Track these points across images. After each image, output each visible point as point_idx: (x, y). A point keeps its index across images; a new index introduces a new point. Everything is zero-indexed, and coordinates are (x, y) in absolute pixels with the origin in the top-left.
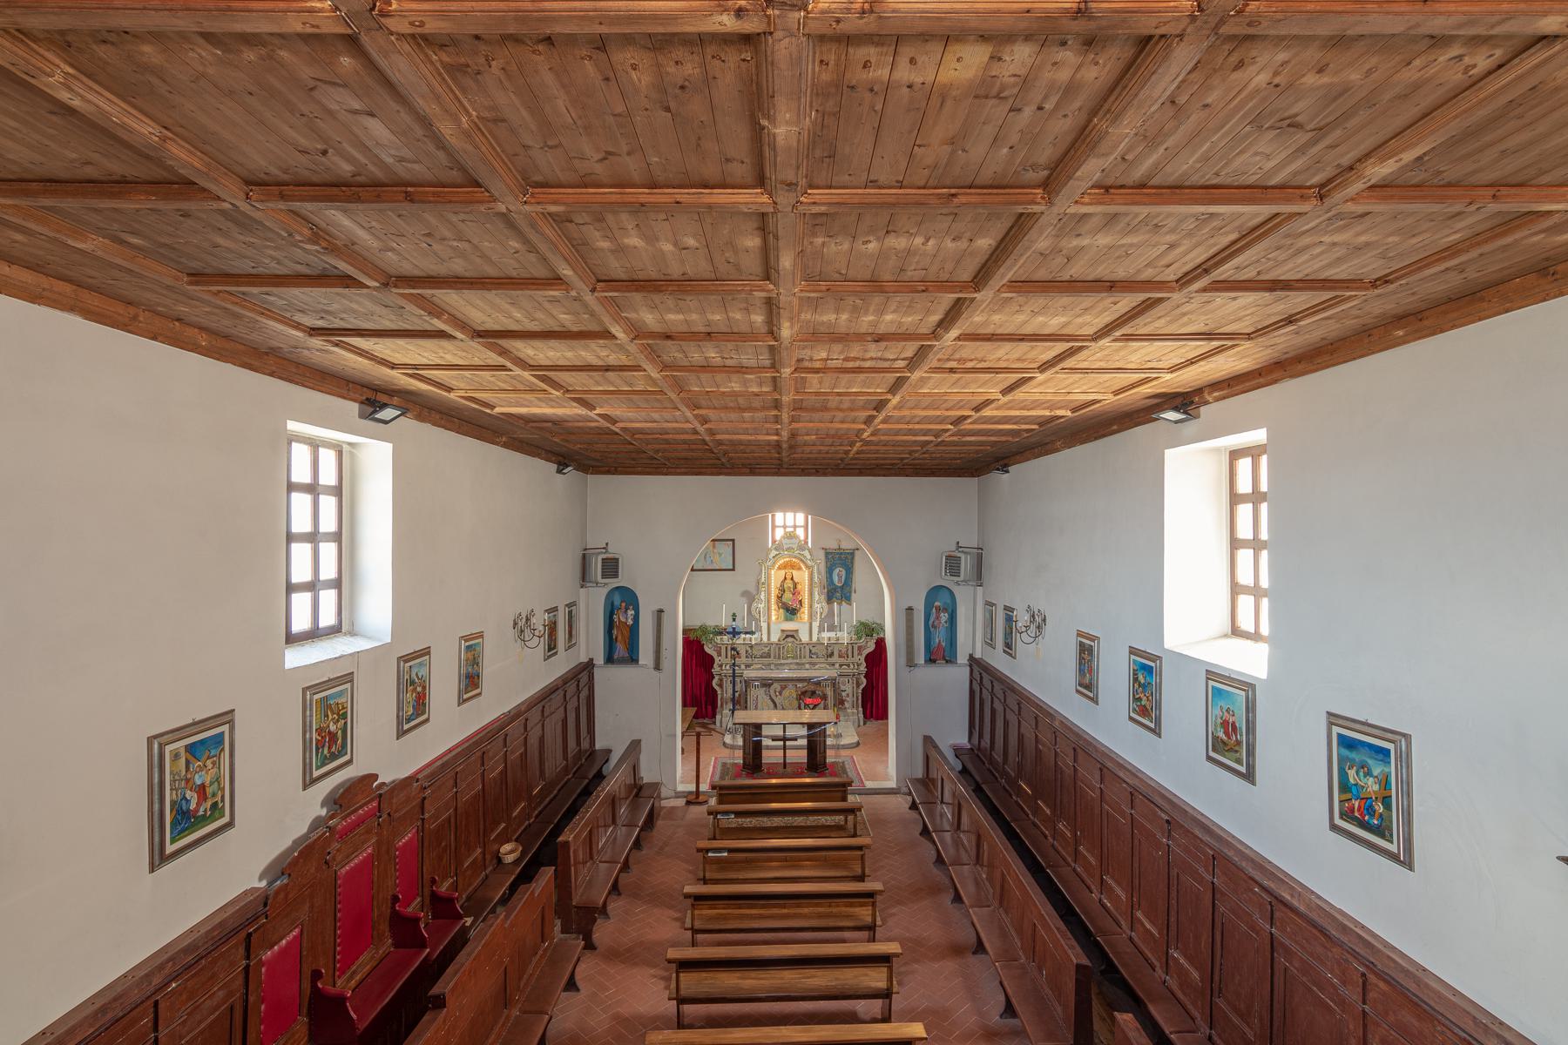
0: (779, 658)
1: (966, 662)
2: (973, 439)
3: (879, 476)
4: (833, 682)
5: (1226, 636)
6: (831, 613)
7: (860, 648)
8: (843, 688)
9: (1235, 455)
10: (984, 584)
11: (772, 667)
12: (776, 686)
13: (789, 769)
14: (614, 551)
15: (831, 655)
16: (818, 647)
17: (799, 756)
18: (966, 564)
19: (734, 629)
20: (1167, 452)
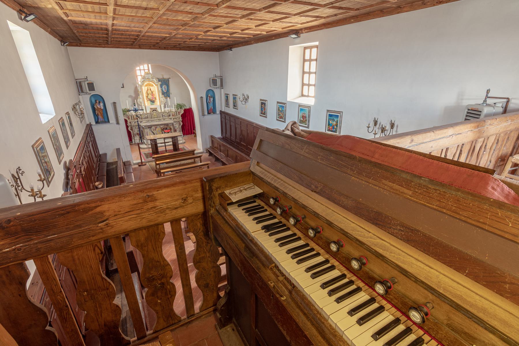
0: (152, 118)
1: (219, 113)
2: (231, 39)
3: (187, 50)
4: (173, 124)
5: (300, 97)
6: (167, 102)
7: (179, 113)
8: (175, 126)
9: (305, 48)
10: (224, 88)
11: (150, 121)
12: (154, 128)
13: (167, 152)
14: (91, 79)
15: (170, 116)
16: (165, 113)
17: (171, 148)
18: (219, 81)
19: (135, 109)
20: (290, 46)
